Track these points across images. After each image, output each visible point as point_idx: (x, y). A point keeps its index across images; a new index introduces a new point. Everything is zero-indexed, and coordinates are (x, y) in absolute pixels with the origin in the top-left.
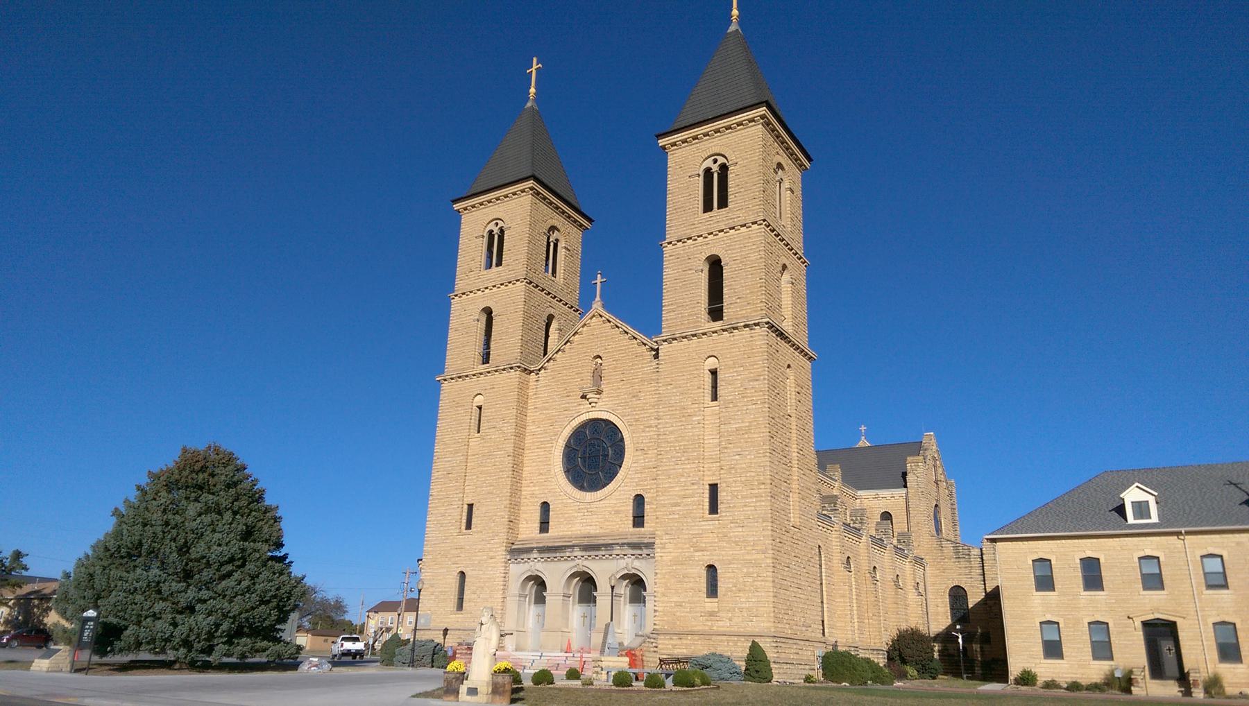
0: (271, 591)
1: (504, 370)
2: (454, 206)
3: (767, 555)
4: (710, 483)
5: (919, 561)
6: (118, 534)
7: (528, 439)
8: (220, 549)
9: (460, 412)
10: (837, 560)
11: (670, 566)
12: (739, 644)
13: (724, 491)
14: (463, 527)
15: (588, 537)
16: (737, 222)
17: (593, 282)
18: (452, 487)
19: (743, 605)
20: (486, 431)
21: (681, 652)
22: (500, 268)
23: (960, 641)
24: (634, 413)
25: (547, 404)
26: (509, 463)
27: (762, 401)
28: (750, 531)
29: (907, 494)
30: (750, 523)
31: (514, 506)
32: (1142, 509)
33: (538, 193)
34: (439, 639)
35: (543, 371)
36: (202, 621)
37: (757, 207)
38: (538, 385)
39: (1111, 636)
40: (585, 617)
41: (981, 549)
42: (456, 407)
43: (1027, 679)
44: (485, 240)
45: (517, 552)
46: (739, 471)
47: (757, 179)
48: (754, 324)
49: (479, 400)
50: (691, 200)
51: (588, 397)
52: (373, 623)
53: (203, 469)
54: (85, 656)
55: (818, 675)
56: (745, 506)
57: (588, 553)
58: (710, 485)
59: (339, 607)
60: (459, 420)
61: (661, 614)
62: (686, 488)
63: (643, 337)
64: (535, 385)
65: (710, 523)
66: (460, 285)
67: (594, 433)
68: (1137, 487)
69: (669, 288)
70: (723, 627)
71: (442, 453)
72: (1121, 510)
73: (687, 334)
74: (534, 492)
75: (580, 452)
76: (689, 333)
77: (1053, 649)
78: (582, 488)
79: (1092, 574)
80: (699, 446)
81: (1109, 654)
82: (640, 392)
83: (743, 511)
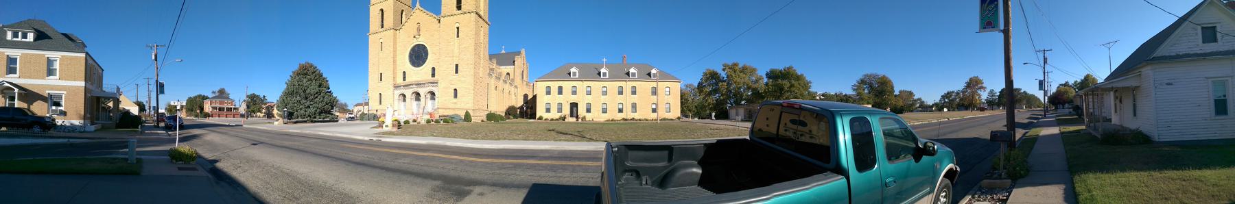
5: (516, 87)
6: (288, 89)
7: (398, 52)
10: (493, 87)
21: (446, 114)
31: (395, 74)
32: (605, 74)
34: (375, 113)
36: (312, 110)
43: (541, 118)
45: (396, 87)
49: (381, 41)
52: (356, 109)
53: (305, 69)
54: (286, 120)
55: (485, 120)
59: (346, 105)
77: (548, 110)
78: (415, 66)
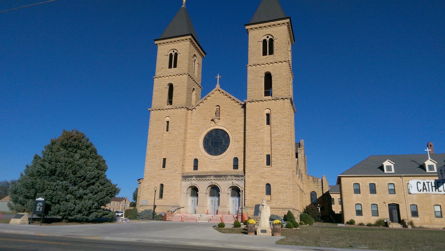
0: (110, 190)
1: (179, 108)
2: (155, 42)
3: (290, 181)
4: (267, 154)
7: (188, 135)
8: (91, 173)
9: (160, 123)
11: (251, 184)
12: (280, 212)
13: (273, 157)
14: (162, 167)
15: (215, 172)
16: (277, 60)
17: (216, 77)
18: (156, 151)
19: (281, 198)
20: (172, 131)
22: (175, 69)
23: (319, 209)
24: (234, 127)
25: (196, 122)
26: (182, 143)
27: (288, 126)
28: (284, 172)
29: (298, 160)
30: (284, 169)
32: (389, 168)
33: (192, 41)
35: (194, 110)
37: (285, 56)
38: (192, 115)
39: (378, 208)
40: (212, 201)
41: (322, 180)
42: (158, 121)
43: (352, 222)
44: (168, 57)
45: (186, 177)
46: (279, 150)
47: (285, 45)
48: (285, 98)
50: (258, 50)
51: (214, 120)
56: (282, 163)
57: (217, 178)
58: (267, 155)
60: (159, 126)
61: (248, 200)
62: (258, 156)
63: (238, 100)
64: (191, 115)
65: (268, 168)
66: (158, 73)
67: (216, 134)
68: (388, 161)
69: (250, 82)
70: (273, 205)
71: (152, 138)
72: (382, 168)
73: (258, 100)
74: (191, 155)
75: (210, 141)
76: (259, 100)
77: (359, 213)
78: (211, 154)
79: (373, 189)
80: (263, 141)
81: (377, 215)
82: (236, 120)
83: (281, 165)
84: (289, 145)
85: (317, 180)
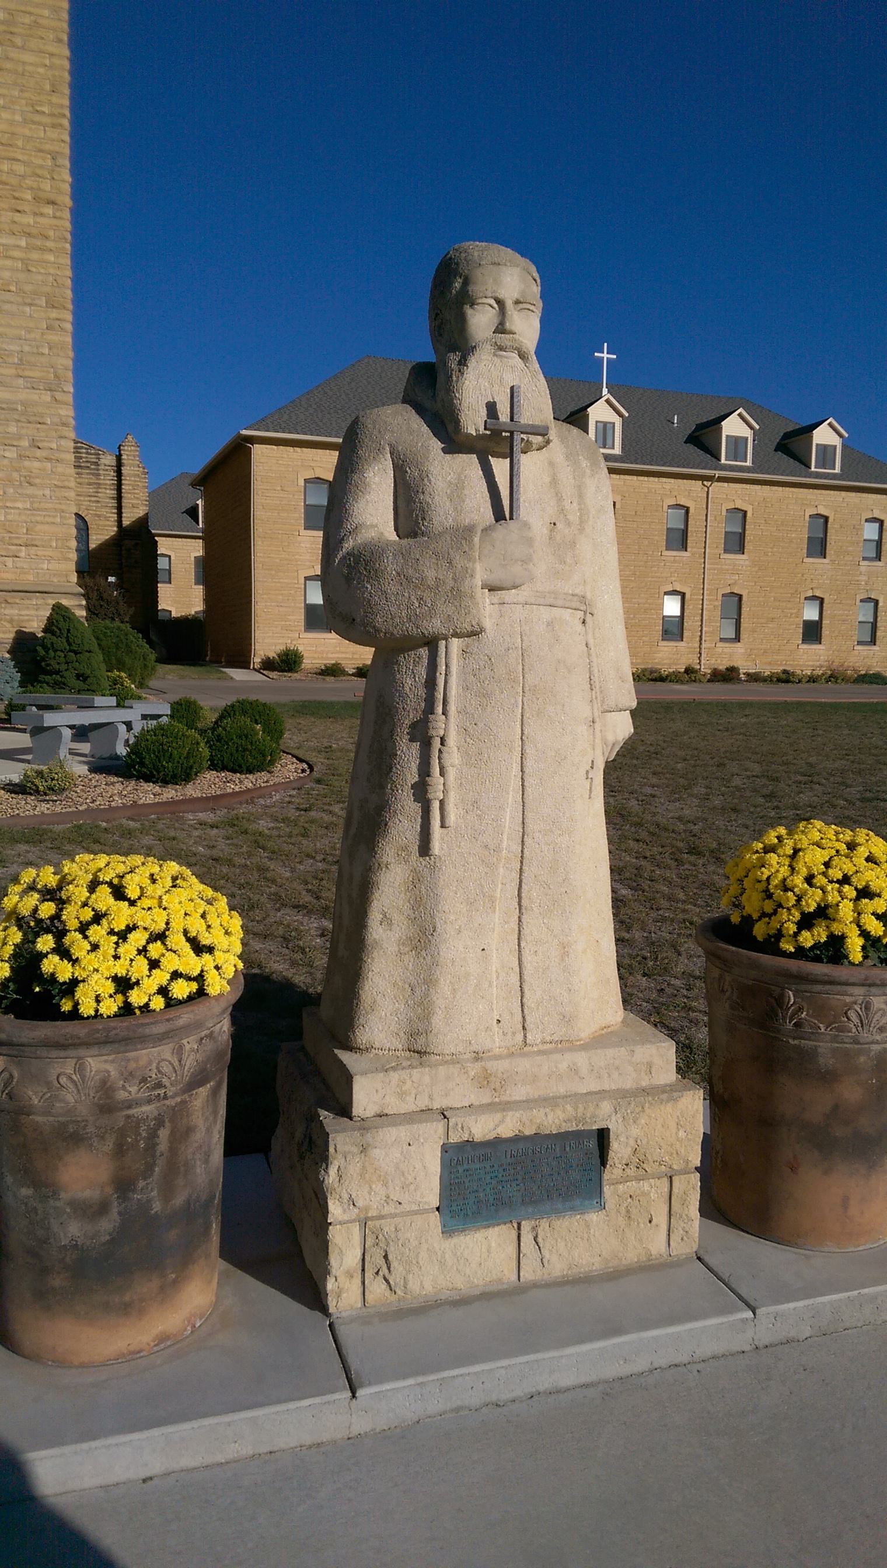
3: (59, 396)
28: (9, 326)
41: (119, 458)
84: (56, 121)
85: (93, 459)
